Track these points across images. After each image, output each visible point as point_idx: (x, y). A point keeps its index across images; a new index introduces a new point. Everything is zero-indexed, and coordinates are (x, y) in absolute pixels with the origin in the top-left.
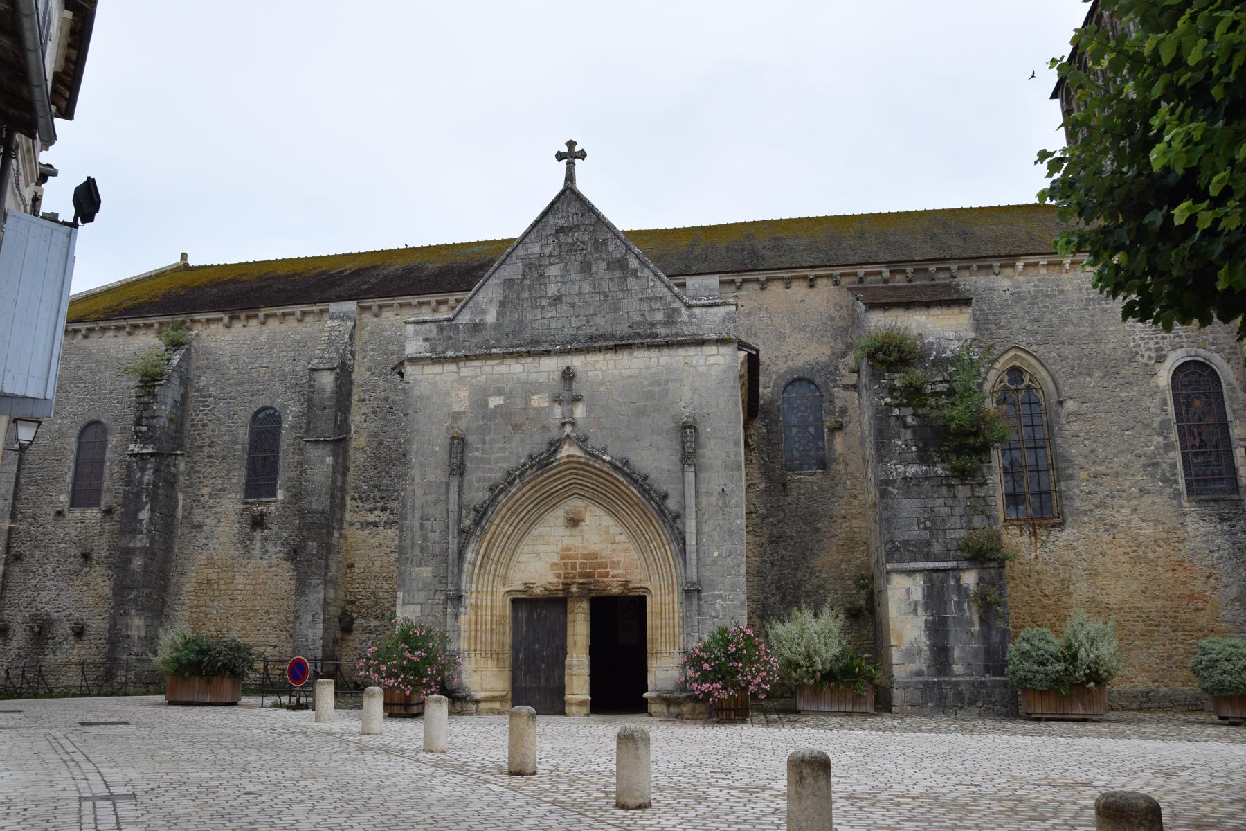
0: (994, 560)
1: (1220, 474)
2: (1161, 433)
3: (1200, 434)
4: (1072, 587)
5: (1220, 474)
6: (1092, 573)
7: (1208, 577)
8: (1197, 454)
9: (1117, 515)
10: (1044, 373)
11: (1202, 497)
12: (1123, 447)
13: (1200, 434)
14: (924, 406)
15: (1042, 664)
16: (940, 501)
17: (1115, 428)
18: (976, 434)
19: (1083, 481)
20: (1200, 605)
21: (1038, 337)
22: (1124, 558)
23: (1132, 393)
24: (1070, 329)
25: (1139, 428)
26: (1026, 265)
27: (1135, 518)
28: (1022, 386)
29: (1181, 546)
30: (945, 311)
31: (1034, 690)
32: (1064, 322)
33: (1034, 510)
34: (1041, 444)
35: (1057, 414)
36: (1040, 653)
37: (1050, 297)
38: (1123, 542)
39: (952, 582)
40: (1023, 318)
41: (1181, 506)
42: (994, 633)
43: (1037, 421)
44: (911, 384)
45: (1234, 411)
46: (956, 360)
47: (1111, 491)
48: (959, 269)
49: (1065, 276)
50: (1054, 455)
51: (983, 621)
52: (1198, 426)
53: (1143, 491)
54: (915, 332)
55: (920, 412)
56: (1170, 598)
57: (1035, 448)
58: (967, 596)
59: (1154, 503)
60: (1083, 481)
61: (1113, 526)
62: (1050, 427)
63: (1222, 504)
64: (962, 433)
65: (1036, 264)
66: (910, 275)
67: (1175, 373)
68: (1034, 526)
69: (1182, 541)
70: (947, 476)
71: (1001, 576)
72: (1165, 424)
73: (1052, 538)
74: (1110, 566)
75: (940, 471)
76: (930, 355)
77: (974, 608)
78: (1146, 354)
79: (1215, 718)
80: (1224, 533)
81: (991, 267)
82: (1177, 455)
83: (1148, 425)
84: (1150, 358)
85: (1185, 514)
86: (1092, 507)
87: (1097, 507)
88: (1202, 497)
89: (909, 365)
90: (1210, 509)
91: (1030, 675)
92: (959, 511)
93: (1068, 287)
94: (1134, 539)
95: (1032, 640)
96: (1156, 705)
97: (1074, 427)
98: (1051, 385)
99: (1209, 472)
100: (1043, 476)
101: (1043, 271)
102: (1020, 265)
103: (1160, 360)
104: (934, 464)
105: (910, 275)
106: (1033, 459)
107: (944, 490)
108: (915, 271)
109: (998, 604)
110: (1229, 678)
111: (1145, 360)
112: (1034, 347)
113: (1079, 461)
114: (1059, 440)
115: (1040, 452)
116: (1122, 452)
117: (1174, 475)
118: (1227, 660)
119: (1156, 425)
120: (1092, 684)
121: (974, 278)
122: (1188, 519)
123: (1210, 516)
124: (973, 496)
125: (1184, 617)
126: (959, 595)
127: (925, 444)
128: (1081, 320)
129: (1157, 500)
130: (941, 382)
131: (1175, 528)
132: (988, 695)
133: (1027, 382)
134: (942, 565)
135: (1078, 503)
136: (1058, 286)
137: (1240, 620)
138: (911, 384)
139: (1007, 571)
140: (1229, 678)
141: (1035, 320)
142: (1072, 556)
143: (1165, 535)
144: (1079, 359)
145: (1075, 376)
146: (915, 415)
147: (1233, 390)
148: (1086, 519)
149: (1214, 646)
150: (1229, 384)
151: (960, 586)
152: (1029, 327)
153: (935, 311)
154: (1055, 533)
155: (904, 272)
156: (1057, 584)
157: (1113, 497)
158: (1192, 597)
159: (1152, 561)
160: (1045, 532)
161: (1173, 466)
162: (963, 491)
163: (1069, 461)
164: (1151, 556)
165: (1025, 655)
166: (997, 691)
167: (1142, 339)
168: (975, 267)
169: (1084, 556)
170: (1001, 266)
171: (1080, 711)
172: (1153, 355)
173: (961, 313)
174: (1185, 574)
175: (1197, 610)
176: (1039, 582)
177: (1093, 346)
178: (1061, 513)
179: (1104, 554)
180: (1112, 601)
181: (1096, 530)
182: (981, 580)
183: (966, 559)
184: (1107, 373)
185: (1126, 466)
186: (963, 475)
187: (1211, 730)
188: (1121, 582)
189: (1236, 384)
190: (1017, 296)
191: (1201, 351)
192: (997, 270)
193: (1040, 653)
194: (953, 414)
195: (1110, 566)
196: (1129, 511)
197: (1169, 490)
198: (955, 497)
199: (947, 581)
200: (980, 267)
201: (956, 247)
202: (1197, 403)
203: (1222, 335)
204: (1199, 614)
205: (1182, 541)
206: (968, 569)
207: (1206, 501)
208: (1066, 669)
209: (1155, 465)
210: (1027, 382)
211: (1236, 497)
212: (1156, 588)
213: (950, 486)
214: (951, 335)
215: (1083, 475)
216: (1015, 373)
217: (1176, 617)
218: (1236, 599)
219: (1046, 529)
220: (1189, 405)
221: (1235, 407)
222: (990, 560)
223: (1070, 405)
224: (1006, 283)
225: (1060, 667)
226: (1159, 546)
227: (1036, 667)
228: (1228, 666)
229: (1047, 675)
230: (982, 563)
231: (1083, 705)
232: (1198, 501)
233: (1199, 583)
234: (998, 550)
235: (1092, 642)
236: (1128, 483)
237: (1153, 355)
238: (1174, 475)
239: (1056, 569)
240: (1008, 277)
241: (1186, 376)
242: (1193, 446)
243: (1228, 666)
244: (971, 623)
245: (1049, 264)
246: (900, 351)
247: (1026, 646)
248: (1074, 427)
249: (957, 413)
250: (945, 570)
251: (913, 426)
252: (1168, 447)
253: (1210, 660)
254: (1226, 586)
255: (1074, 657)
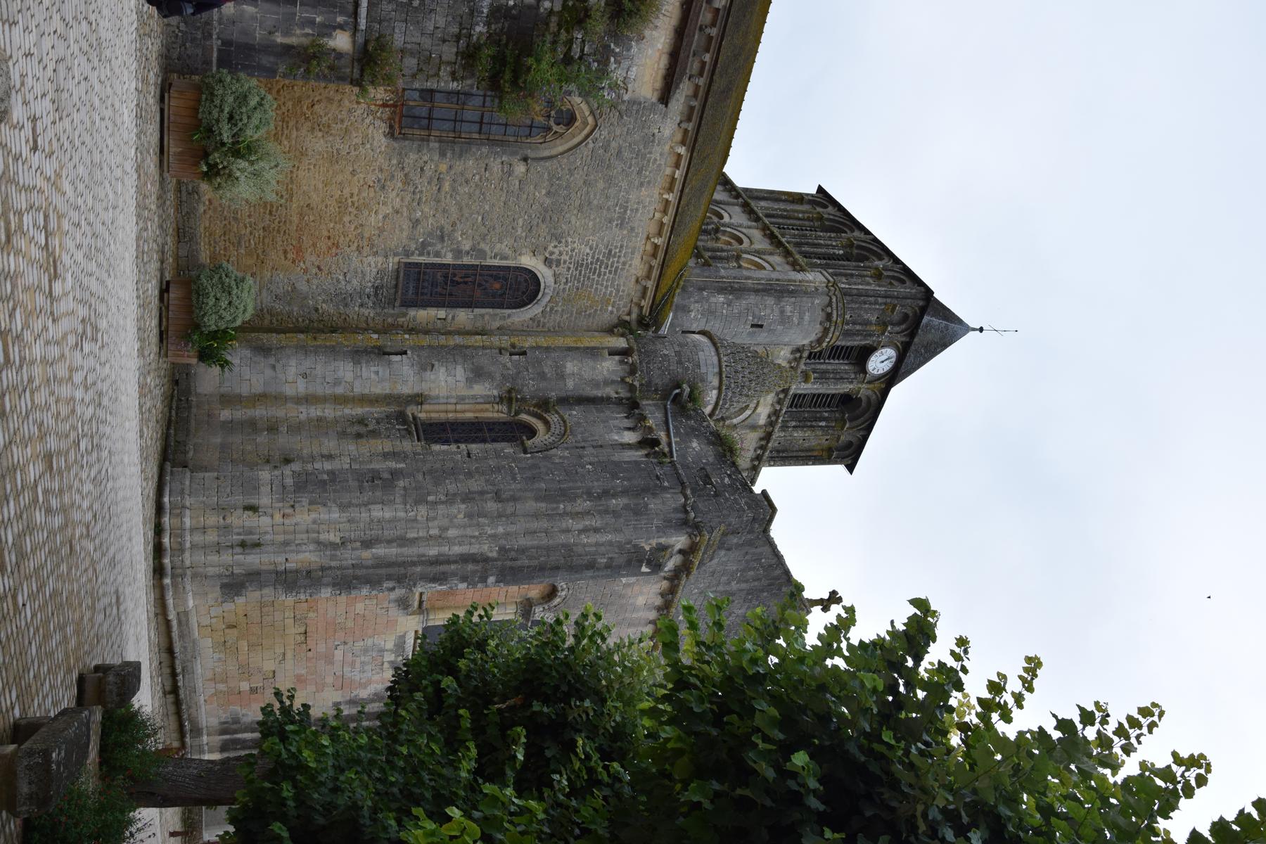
0: (362, 75)
1: (422, 294)
2: (473, 249)
3: (466, 283)
4: (320, 134)
5: (422, 294)
6: (334, 158)
7: (319, 268)
8: (446, 277)
9: (394, 193)
10: (561, 149)
11: (402, 275)
12: (466, 212)
13: (466, 283)
14: (560, 26)
15: (231, 118)
16: (441, 23)
17: (487, 207)
18: (514, 82)
19: (437, 166)
20: (290, 256)
21: (601, 151)
22: (346, 192)
23: (520, 230)
24: (601, 185)
25: (483, 230)
26: (679, 155)
27: (389, 210)
28: (552, 123)
29: (354, 247)
30: (662, 72)
31: (199, 101)
32: (609, 181)
33: (413, 107)
34: (485, 128)
35: (514, 153)
36: (245, 117)
37: (639, 173)
38: (365, 194)
39: (340, 19)
40: (625, 141)
41: (395, 255)
42: (272, 59)
43: (510, 130)
44: (589, 17)
45: (482, 316)
46: (603, 72)
47: (421, 192)
48: (697, 87)
49: (656, 191)
50: (470, 142)
51: (288, 49)
52: (474, 283)
53: (416, 223)
54: (647, 33)
55: (554, 19)
56: (299, 229)
57: (481, 123)
58: (323, 35)
59: (402, 230)
60: (437, 166)
61: (383, 187)
62: (501, 143)
63: (393, 291)
64: (519, 72)
65: (677, 166)
66: (708, 31)
67: (530, 271)
68: (394, 106)
69: (359, 249)
70: (470, 35)
71: (341, 79)
72: (482, 254)
73: (378, 123)
74: (340, 178)
75: (478, 29)
76: (617, 45)
77: (305, 41)
78: (556, 251)
79: (168, 277)
80: (363, 288)
81: (689, 119)
82: (448, 259)
83: (484, 239)
84: (552, 253)
85: (386, 257)
86: (406, 170)
87: (406, 175)
88: (402, 275)
89: (611, 18)
90: (388, 280)
91: (217, 102)
92: (427, 43)
93: (644, 191)
94: (366, 206)
95: (261, 104)
96: (184, 198)
97: (496, 167)
98: (546, 153)
99: (426, 284)
100: (448, 125)
101: (668, 171)
102: (682, 150)
103: (547, 262)
104: (488, 24)
105: (708, 31)
106: (469, 118)
107: (454, 29)
108: (710, 38)
109: (308, 71)
110: (211, 303)
111: (550, 248)
112: (591, 145)
113: (459, 166)
114: (485, 150)
115: (476, 127)
116: (461, 209)
117: (429, 254)
118: (230, 303)
119: (482, 246)
120: (205, 169)
121: (682, 100)
122: (380, 259)
123: (382, 279)
124: (441, 62)
125: (279, 239)
126: (323, 25)
127: (514, 18)
128: (607, 197)
129: (405, 234)
130: (582, 50)
131: (373, 246)
132: (193, 40)
133: (555, 128)
134: (363, 11)
135: (413, 156)
136: (649, 182)
137: (273, 288)
138: (589, 17)
139: (348, 88)
140: (211, 303)
141: (619, 152)
142: (356, 141)
143: (366, 235)
144: (568, 187)
145: (550, 180)
146: (551, 12)
147: (504, 318)
148: (394, 162)
149: (246, 292)
150: (509, 316)
151: (335, 28)
152: (613, 144)
153: (664, 61)
154: (384, 128)
155: (713, 25)
156: (325, 119)
157: (414, 193)
158: (299, 250)
159: (341, 219)
160: (385, 116)
161: (437, 254)
162: (449, 52)
163: (460, 156)
164: (346, 219)
165: (243, 99)
166: (199, 51)
167: (573, 250)
168: (694, 103)
169: (353, 153)
170: (686, 131)
171: (173, 148)
172: (554, 257)
173: (654, 90)
174: (324, 248)
175: (285, 252)
176: (330, 100)
177: (577, 203)
178: (405, 137)
179: (353, 173)
180: (301, 173)
181: (381, 170)
182: (339, 55)
183: (366, 42)
184: (546, 211)
185: (444, 211)
186: (469, 56)
187: (154, 267)
188: (320, 186)
189: (509, 321)
190: (650, 140)
191: (547, 298)
192: (684, 125)
193: (245, 117)
194: (544, 66)
195: (340, 178)
196: (397, 206)
197: (413, 246)
198: (444, 41)
199: (341, 13)
200: (692, 108)
201: (719, 84)
202: (497, 286)
203: (558, 319)
204: (281, 253)
205: (359, 249)
206: (354, 42)
207: (397, 278)
208: (223, 144)
209: (442, 238)
210: (555, 128)
211: (397, 304)
212: (312, 218)
213: (458, 37)
214: (632, 74)
215: (443, 167)
216: (569, 119)
217: (279, 231)
218: (294, 288)
219: (389, 119)
220: (496, 278)
221: (487, 317)
222: (362, 71)
223: (520, 168)
224: (667, 132)
225: (226, 137)
226: (356, 228)
227: (227, 110)
228: (224, 304)
229: (218, 121)
230: (359, 60)
231: (180, 154)
232: (398, 271)
233: (313, 258)
234: (372, 83)
235: (256, 174)
236: (426, 210)
237: (554, 257)
238: (429, 254)
239: (342, 121)
240: (673, 135)
241: (526, 281)
242: (455, 275)
243: (224, 304)
244: (287, 33)
245: (673, 180)
246: (630, 14)
247: (253, 102)
248: (496, 167)
249: (544, 68)
250: (356, 14)
251: (538, 7)
252: (458, 253)
253: (229, 286)
254: (308, 281)
255: (237, 154)
